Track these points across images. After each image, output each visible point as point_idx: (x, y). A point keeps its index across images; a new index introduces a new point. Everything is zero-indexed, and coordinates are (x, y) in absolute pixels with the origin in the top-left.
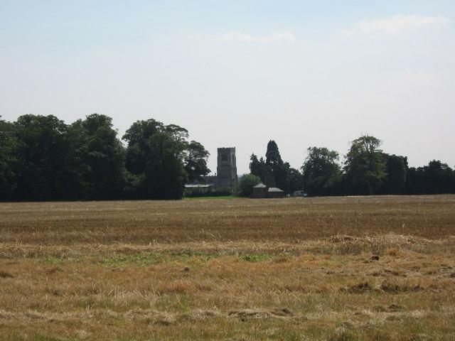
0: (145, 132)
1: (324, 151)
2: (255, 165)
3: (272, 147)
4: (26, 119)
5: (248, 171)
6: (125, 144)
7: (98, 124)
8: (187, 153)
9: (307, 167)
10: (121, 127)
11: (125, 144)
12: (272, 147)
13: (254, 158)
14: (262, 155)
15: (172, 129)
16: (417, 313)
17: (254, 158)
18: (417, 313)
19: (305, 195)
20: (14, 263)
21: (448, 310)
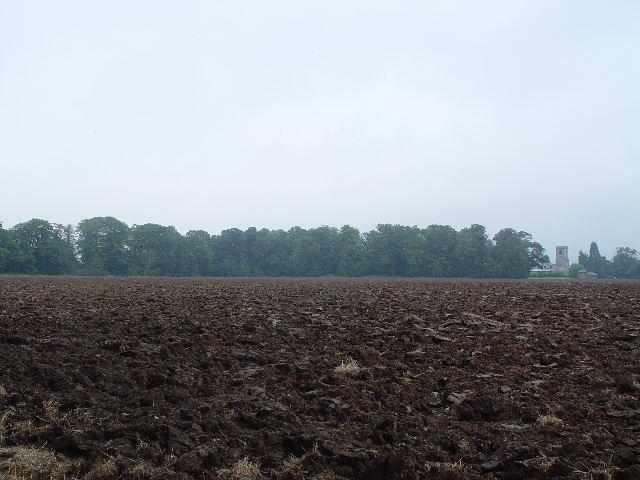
0: (506, 235)
1: (627, 249)
2: (582, 257)
3: (594, 247)
4: (433, 227)
5: (577, 262)
6: (495, 243)
7: (478, 230)
8: (530, 249)
9: (615, 259)
10: (491, 233)
11: (495, 243)
12: (594, 247)
13: (581, 253)
14: (587, 251)
15: (522, 234)
16: (375, 451)
17: (581, 253)
18: (375, 451)
19: (462, 258)
20: (252, 343)
21: (638, 411)
